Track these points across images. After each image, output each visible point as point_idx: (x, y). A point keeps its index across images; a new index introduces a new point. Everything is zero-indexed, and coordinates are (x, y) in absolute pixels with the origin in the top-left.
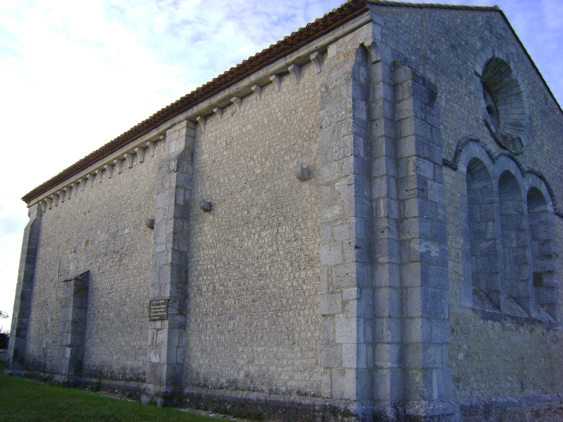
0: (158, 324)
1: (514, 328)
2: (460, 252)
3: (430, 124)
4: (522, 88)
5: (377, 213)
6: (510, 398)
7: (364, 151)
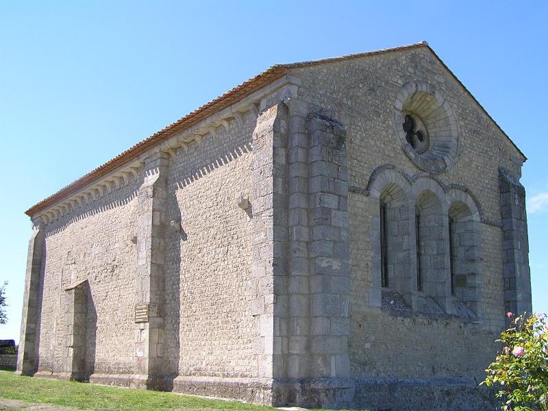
0: (142, 325)
4: (449, 113)
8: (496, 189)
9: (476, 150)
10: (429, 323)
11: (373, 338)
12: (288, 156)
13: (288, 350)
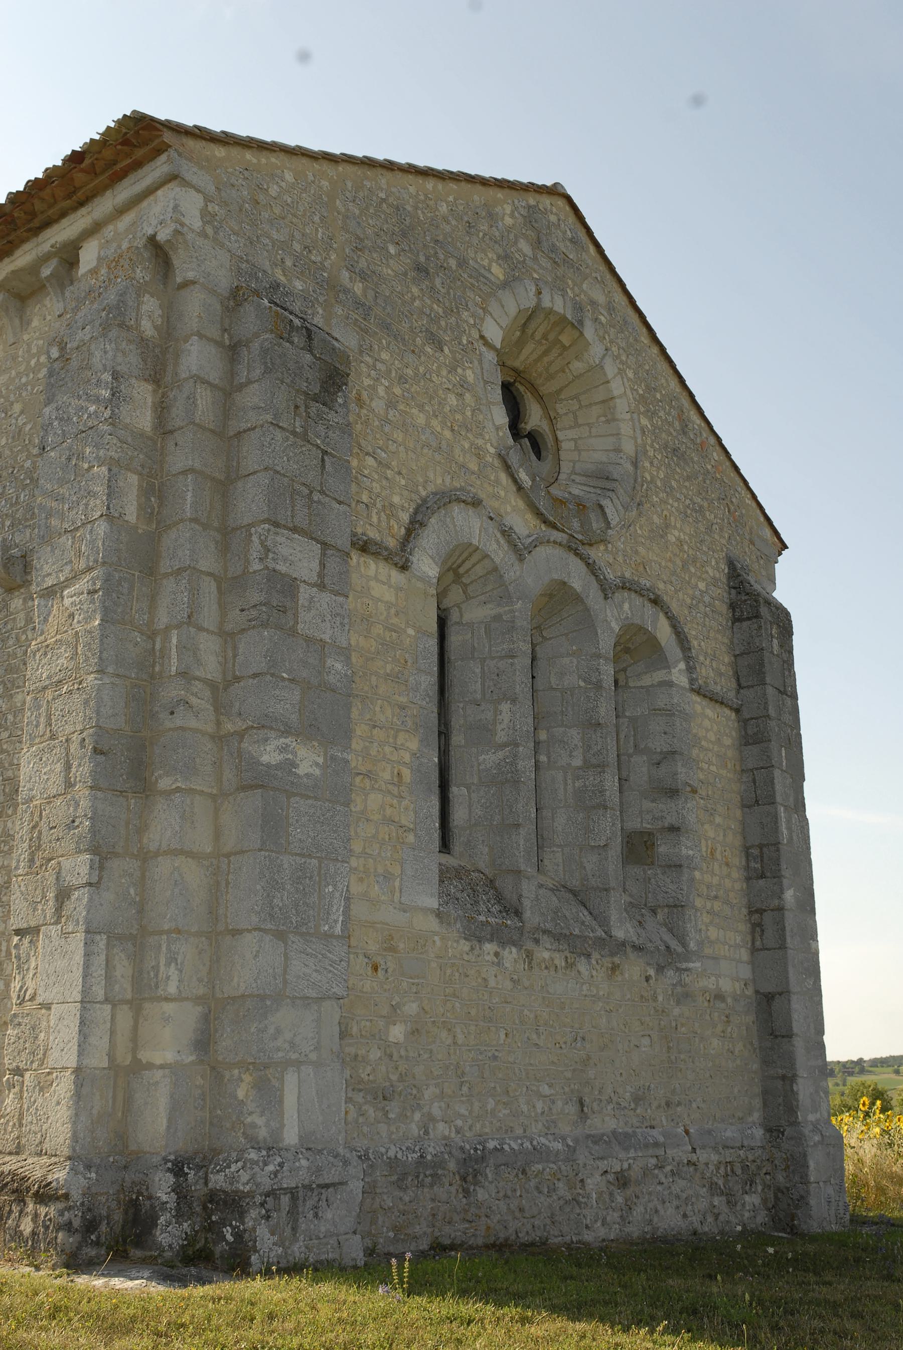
1: (559, 961)
2: (406, 773)
3: (318, 447)
4: (617, 387)
5: (162, 665)
6: (543, 1140)
7: (140, 507)
8: (723, 608)
9: (678, 500)
10: (570, 965)
11: (412, 1008)
12: (162, 409)
13: (134, 1050)
